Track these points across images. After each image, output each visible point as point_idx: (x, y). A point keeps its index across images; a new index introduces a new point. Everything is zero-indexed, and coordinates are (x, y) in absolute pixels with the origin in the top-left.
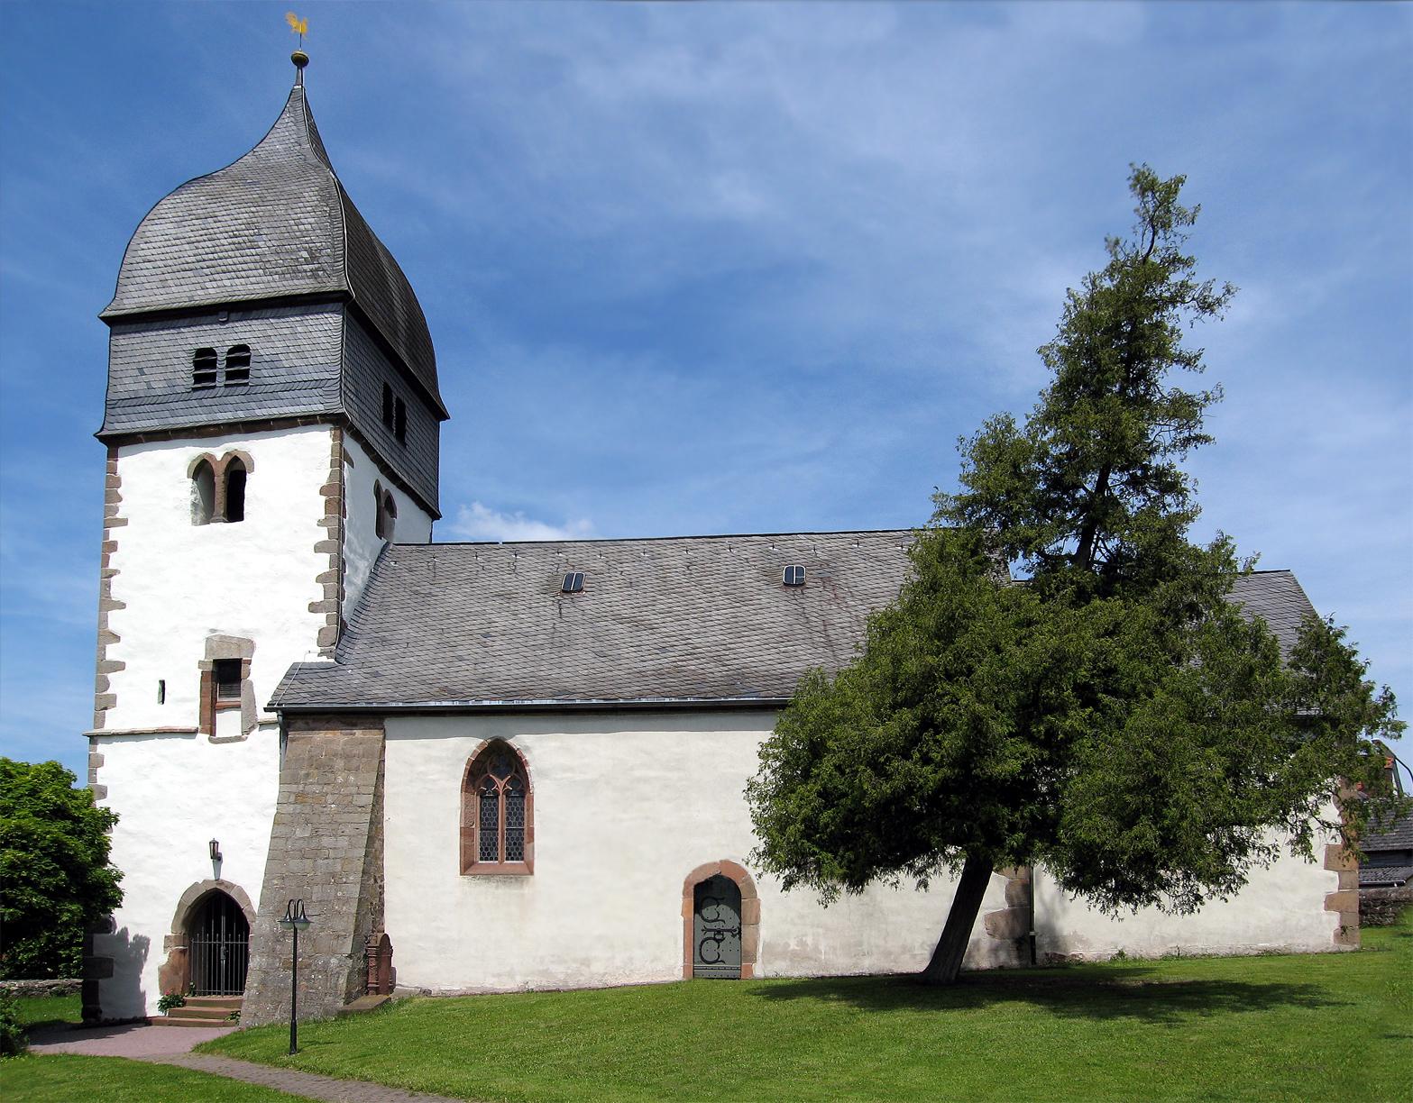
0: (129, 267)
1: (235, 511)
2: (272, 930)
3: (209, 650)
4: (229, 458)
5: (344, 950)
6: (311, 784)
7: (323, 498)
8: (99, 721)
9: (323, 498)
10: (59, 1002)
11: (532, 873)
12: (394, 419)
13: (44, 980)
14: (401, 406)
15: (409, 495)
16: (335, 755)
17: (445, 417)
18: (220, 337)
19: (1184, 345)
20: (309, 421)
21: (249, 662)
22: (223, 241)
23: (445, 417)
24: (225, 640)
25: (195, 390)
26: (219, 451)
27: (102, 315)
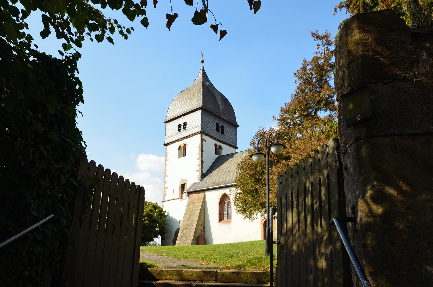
0: (169, 113)
1: (185, 155)
2: (180, 236)
3: (181, 182)
4: (184, 144)
5: (191, 239)
6: (191, 206)
7: (199, 149)
8: (164, 199)
9: (199, 149)
10: (143, 249)
11: (231, 221)
12: (220, 130)
13: (18, 234)
14: (222, 127)
15: (227, 145)
16: (195, 200)
17: (238, 126)
18: (181, 121)
19: (332, 62)
20: (196, 134)
21: (187, 184)
22: (183, 103)
23: (238, 126)
24: (183, 180)
25: (178, 132)
26: (182, 143)
27: (164, 122)
